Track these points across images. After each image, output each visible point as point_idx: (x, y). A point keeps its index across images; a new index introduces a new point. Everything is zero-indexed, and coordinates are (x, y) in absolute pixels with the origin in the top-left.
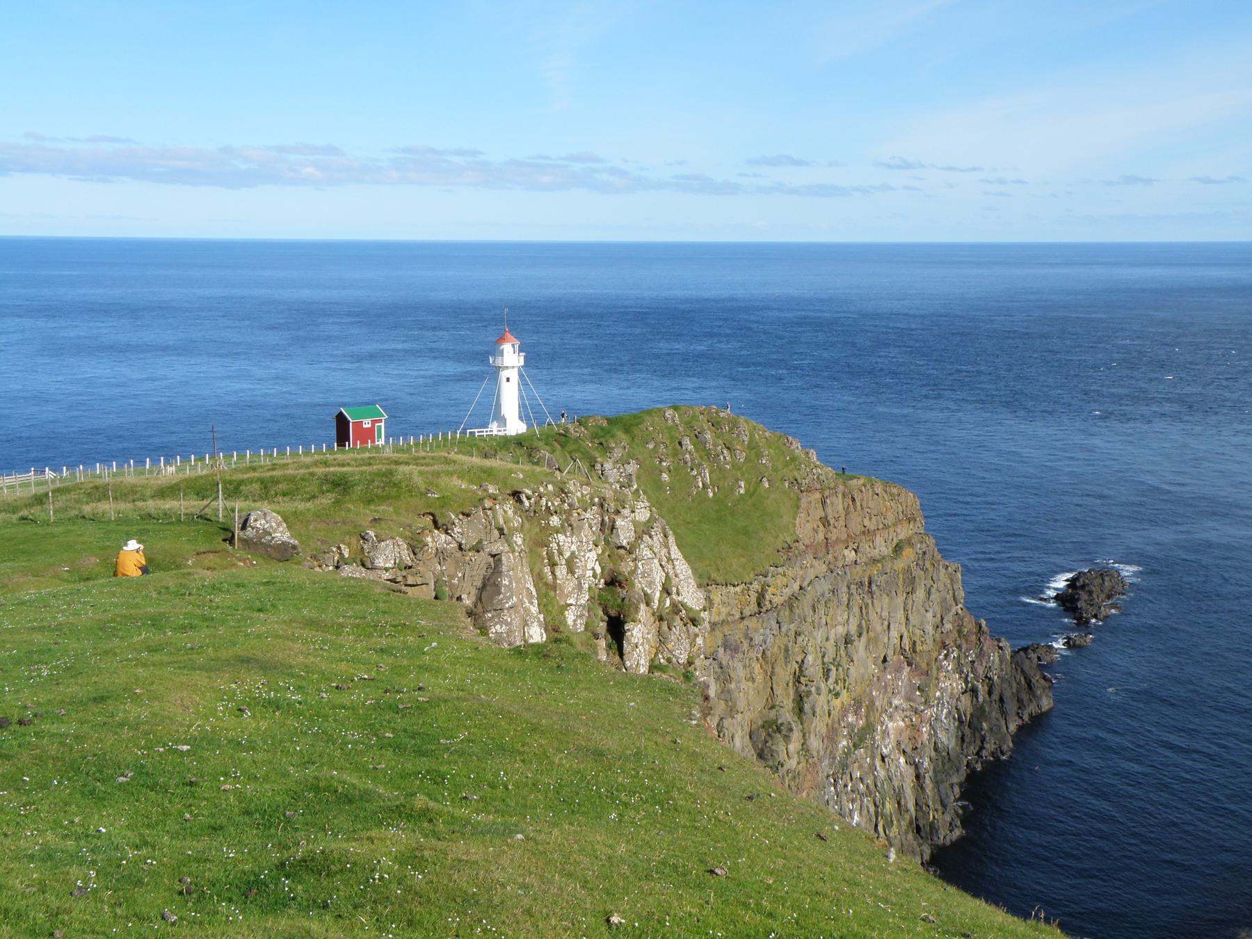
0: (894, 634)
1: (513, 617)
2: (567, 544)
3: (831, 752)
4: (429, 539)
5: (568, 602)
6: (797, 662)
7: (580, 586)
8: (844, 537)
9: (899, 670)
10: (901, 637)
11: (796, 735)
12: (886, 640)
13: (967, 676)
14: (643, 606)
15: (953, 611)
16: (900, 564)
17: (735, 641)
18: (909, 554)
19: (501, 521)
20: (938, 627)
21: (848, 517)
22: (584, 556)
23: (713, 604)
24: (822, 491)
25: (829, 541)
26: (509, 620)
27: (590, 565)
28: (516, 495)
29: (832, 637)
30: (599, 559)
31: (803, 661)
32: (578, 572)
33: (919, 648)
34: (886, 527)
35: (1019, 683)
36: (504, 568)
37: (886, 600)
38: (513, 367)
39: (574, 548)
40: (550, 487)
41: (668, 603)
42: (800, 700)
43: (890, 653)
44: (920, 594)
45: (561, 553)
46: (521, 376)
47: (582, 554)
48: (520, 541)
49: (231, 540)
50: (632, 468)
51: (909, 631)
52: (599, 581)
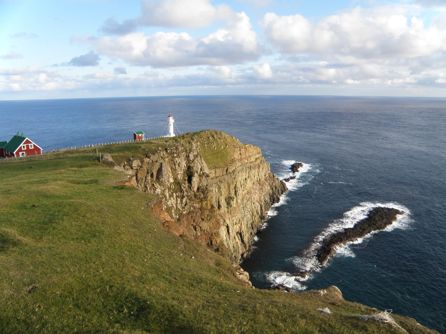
0: (256, 178)
4: (145, 160)
7: (181, 170)
8: (245, 157)
9: (257, 185)
11: (235, 200)
14: (196, 173)
15: (268, 172)
16: (257, 163)
18: (258, 161)
19: (162, 155)
24: (240, 147)
27: (184, 165)
28: (166, 150)
30: (186, 163)
32: (181, 166)
33: (261, 180)
34: (253, 155)
36: (163, 166)
39: (180, 161)
40: (174, 148)
42: (236, 192)
43: (255, 182)
44: (261, 169)
45: (176, 162)
48: (167, 160)
49: (99, 161)
50: (199, 143)
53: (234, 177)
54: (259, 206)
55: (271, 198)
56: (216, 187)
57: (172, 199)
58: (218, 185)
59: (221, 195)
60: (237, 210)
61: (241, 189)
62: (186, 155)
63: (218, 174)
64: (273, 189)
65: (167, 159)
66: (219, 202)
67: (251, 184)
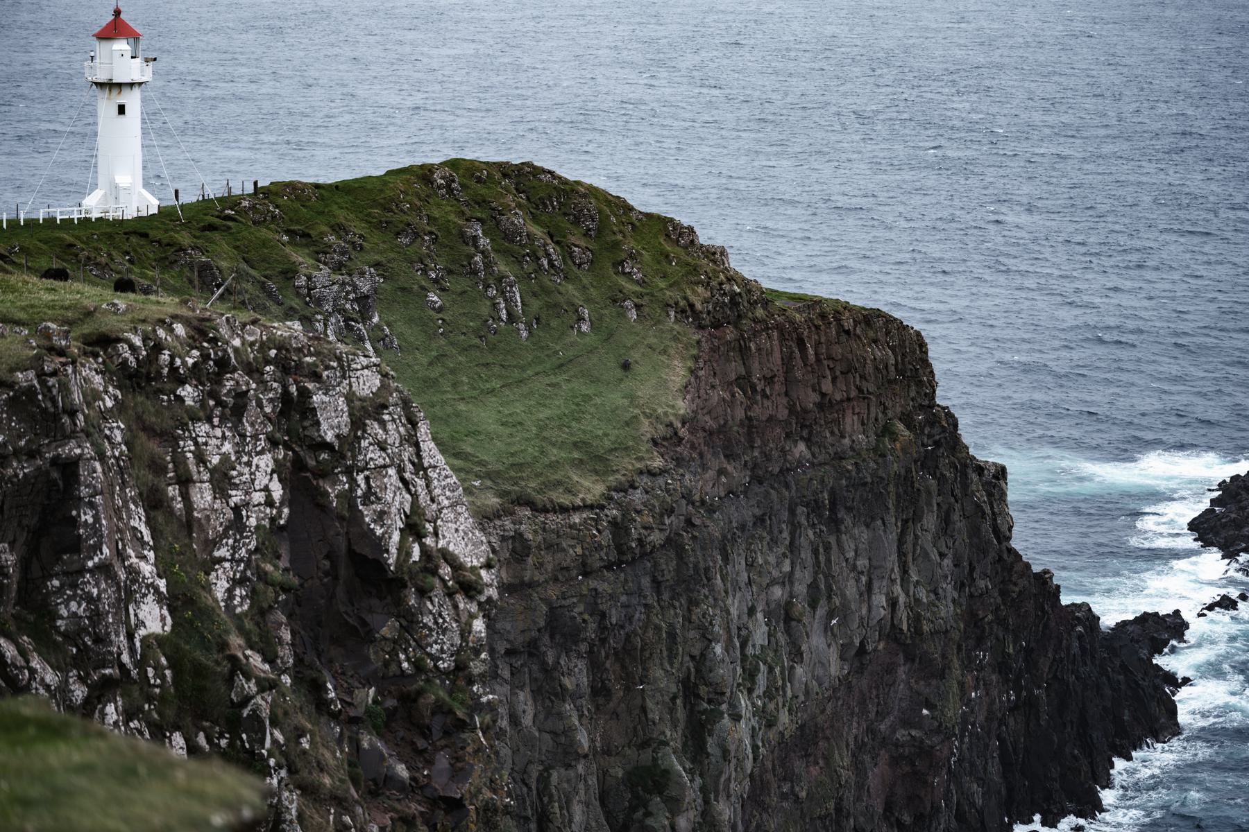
5: (217, 554)
20: (963, 585)
22: (249, 464)
26: (95, 591)
40: (180, 329)
45: (201, 459)
47: (245, 459)
61: (743, 701)
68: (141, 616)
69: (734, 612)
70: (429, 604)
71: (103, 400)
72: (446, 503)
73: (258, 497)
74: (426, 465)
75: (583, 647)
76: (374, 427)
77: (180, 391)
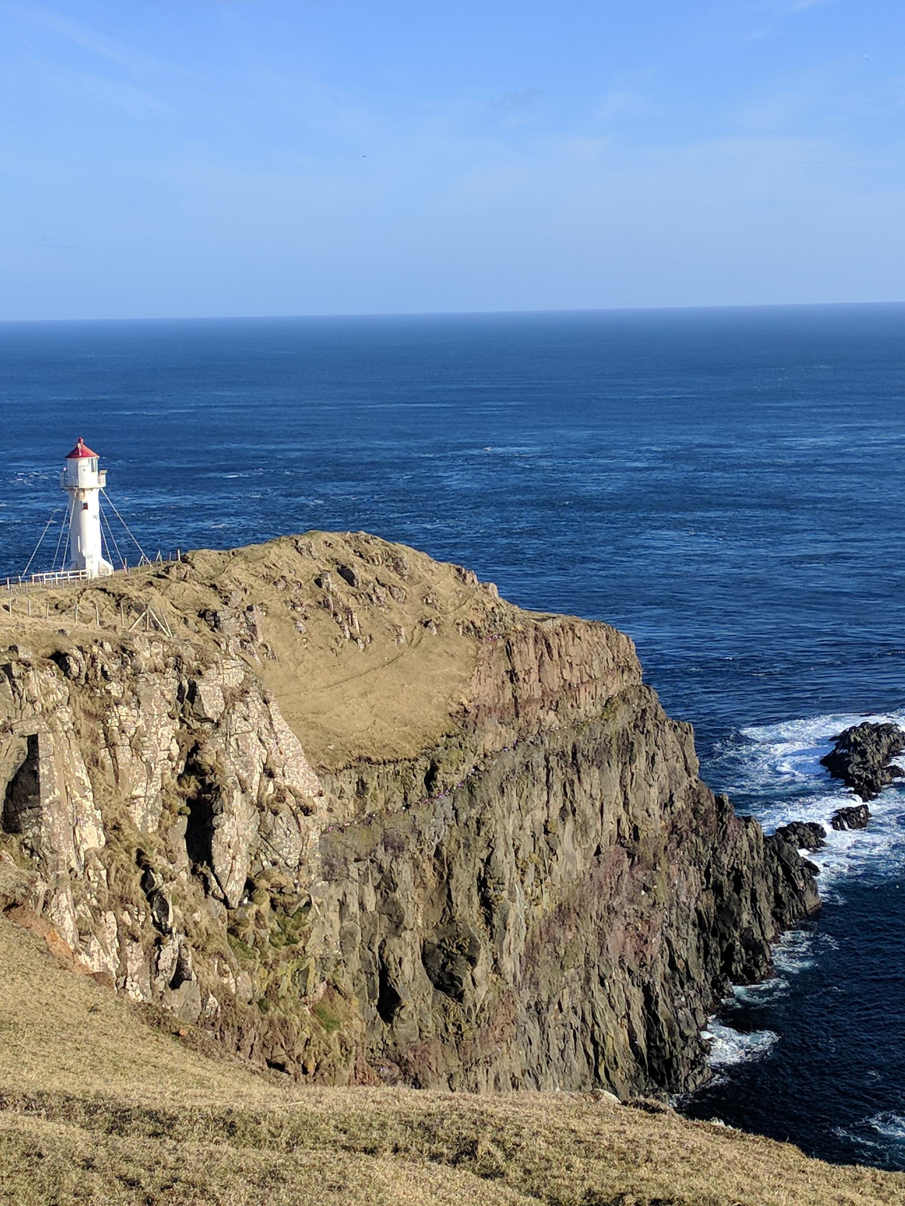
1: (56, 816)
2: (131, 719)
3: (532, 975)
5: (135, 793)
6: (482, 860)
8: (537, 694)
10: (619, 821)
11: (484, 958)
12: (599, 826)
13: (709, 867)
15: (685, 783)
17: (399, 836)
20: (666, 805)
21: (542, 669)
22: (156, 733)
23: (368, 789)
25: (519, 700)
26: (51, 819)
27: (165, 743)
29: (527, 824)
31: (489, 859)
32: (147, 754)
35: (776, 875)
36: (41, 754)
37: (595, 771)
38: (92, 489)
39: (141, 722)
41: (271, 789)
44: (641, 763)
46: (102, 500)
47: (154, 730)
51: (628, 813)
52: (177, 765)
53: (473, 812)
54: (637, 996)
55: (713, 944)
56: (364, 877)
57: (94, 946)
58: (380, 869)
59: (397, 925)
60: (500, 1020)
62: (180, 687)
63: (374, 796)
64: (718, 889)
65: (65, 715)
66: (384, 973)
67: (579, 855)
68: (84, 836)
69: (510, 829)
70: (280, 821)
71: (56, 694)
72: (291, 754)
73: (164, 755)
74: (276, 730)
75: (407, 856)
76: (240, 706)
77: (108, 687)
